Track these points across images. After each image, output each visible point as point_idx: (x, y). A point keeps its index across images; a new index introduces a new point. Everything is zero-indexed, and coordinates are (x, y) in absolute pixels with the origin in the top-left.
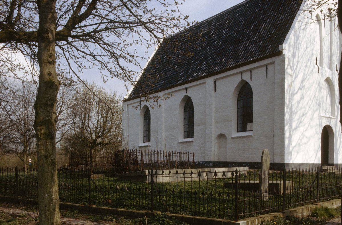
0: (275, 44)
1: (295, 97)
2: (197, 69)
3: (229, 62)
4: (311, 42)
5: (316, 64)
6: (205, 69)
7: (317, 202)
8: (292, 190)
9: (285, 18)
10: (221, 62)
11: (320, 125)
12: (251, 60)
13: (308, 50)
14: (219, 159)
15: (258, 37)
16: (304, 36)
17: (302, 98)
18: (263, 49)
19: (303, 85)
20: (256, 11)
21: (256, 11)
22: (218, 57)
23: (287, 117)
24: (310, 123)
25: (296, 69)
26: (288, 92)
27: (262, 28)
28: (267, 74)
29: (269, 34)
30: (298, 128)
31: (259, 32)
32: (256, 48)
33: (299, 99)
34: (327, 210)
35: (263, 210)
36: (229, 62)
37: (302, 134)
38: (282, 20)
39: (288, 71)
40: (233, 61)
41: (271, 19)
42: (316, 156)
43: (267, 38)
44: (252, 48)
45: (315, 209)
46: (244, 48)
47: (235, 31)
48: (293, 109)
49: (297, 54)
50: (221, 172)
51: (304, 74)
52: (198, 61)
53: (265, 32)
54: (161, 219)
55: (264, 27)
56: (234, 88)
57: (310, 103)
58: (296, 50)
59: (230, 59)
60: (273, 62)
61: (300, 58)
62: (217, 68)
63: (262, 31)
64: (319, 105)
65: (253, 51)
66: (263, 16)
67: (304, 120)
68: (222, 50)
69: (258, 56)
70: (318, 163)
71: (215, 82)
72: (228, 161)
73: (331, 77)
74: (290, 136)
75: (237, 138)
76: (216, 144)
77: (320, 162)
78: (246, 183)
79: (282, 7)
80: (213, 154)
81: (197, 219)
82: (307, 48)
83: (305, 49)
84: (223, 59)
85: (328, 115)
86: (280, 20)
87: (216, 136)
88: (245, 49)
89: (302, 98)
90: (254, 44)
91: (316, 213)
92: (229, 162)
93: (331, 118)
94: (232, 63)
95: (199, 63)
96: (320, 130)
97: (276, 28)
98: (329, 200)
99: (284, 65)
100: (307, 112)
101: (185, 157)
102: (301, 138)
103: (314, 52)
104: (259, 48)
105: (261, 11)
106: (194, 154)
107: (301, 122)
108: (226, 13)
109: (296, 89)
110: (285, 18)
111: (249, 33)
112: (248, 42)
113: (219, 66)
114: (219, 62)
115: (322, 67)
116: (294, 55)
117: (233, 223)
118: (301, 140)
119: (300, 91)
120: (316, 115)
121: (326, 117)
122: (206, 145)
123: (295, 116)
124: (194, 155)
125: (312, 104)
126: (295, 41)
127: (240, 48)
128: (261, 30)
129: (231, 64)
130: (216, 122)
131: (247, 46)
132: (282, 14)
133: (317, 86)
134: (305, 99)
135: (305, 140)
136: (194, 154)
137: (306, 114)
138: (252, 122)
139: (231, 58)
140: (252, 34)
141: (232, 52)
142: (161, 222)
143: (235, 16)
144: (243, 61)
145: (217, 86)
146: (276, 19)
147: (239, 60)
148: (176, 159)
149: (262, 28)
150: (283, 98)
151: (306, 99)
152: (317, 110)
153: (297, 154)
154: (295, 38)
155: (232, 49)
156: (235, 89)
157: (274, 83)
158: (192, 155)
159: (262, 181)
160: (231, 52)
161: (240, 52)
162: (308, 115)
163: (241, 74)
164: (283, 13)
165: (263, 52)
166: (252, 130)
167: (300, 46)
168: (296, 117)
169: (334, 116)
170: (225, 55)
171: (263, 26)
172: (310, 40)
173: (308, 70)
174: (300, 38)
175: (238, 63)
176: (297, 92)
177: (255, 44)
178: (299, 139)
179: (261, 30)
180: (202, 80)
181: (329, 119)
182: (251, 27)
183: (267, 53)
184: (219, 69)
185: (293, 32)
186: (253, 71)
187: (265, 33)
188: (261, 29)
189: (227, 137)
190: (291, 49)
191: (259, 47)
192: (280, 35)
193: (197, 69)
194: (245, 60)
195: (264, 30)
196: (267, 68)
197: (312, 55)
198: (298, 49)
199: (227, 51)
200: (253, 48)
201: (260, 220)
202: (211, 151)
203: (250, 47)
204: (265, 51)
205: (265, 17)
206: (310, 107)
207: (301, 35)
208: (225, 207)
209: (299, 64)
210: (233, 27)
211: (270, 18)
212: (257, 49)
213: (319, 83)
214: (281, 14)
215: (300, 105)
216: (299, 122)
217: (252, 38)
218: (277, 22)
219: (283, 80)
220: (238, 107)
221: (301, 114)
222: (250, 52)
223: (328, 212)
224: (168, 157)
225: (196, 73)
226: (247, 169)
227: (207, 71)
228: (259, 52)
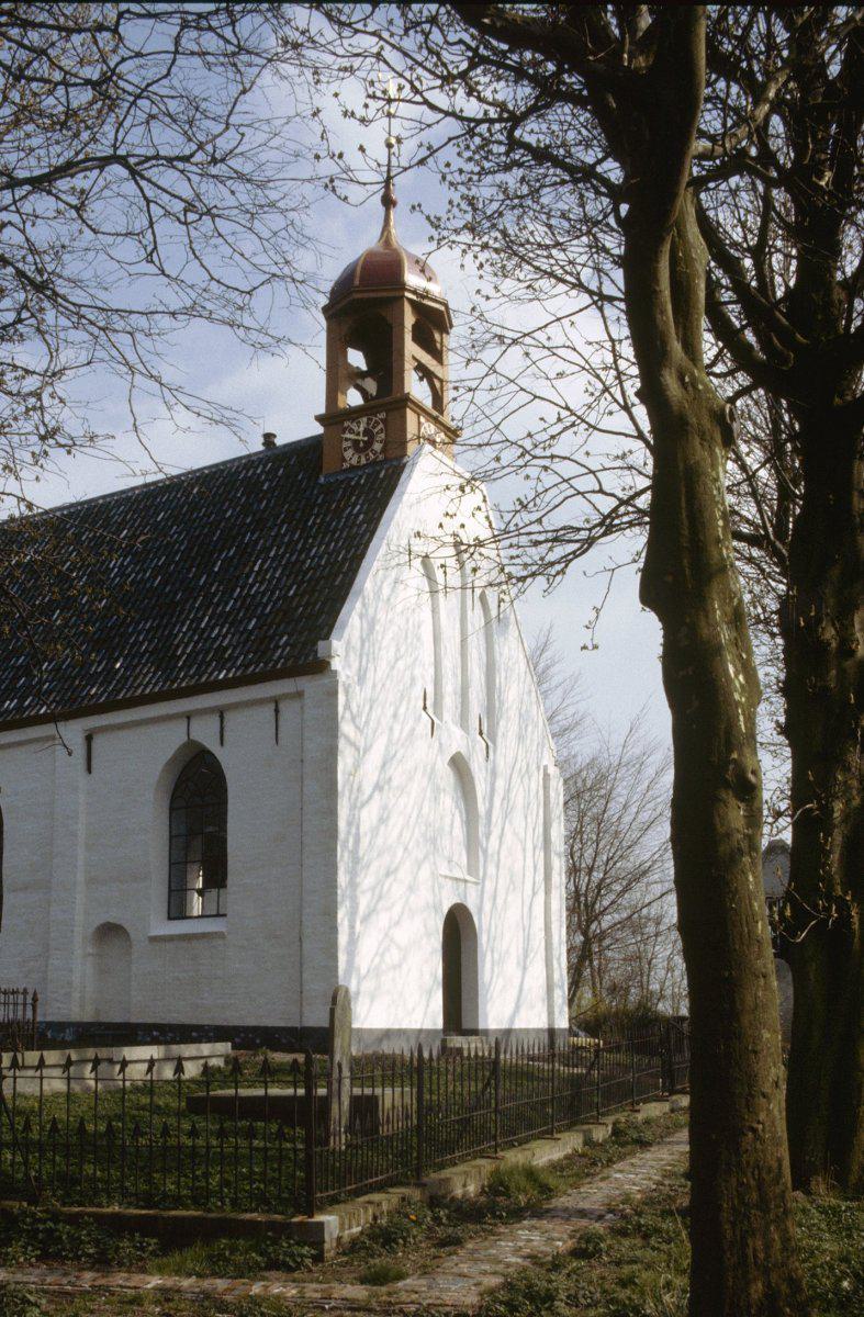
0: (301, 633)
1: (364, 814)
2: (18, 686)
3: (139, 674)
4: (409, 641)
5: (425, 708)
6: (49, 692)
7: (496, 1152)
8: (400, 1124)
9: (330, 554)
10: (110, 671)
11: (436, 908)
12: (221, 676)
13: (401, 664)
14: (97, 1011)
15: (239, 603)
16: (390, 621)
17: (383, 820)
18: (261, 643)
19: (387, 777)
20: (229, 514)
21: (229, 514)
22: (98, 652)
23: (342, 878)
24: (407, 901)
25: (367, 723)
26: (347, 793)
27: (253, 576)
28: (277, 729)
29: (278, 599)
30: (374, 917)
31: (242, 588)
32: (237, 637)
33: (375, 821)
34: (530, 1174)
35: (371, 1181)
36: (139, 674)
37: (386, 935)
38: (321, 558)
39: (346, 728)
40: (155, 673)
41: (282, 550)
42: (428, 1005)
43: (274, 610)
44: (223, 636)
45: (496, 1172)
46: (194, 634)
47: (157, 570)
48: (361, 853)
49: (370, 674)
50: (144, 1061)
51: (390, 740)
52: (18, 659)
53: (263, 588)
54: (41, 1227)
55: (258, 573)
56: (160, 768)
57: (406, 835)
58: (368, 661)
59: (145, 665)
60: (298, 692)
61: (378, 689)
62: (94, 689)
63: (252, 586)
64: (433, 841)
65: (226, 649)
66: (252, 534)
67: (389, 890)
68: (111, 628)
69: (247, 667)
70: (428, 1025)
71: (89, 739)
72: (134, 1020)
73: (464, 751)
74: (353, 941)
75: (171, 938)
76: (90, 958)
77: (440, 1024)
78: (242, 1099)
79: (317, 516)
80: (76, 995)
81: (176, 1217)
82: (397, 660)
83: (393, 661)
84: (117, 661)
85: (459, 875)
86: (313, 559)
87: (91, 930)
88: (196, 638)
89: (383, 820)
90: (227, 625)
91: (502, 1184)
92: (138, 1026)
93: (466, 881)
94: (149, 680)
95: (21, 665)
96: (437, 925)
97: (302, 582)
98: (516, 1144)
99: (335, 706)
100: (400, 863)
101: (20, 1008)
102: (381, 951)
103: (417, 672)
104: (247, 640)
105: (246, 516)
106: (35, 994)
107: (380, 897)
108: (119, 503)
109: (367, 790)
110: (330, 554)
111: (209, 584)
112: (204, 615)
113: (101, 685)
114: (103, 669)
115: (494, 743)
116: (361, 679)
117: (301, 1223)
118: (383, 955)
119: (377, 795)
120: (425, 873)
121: (451, 878)
122: (51, 961)
123: (365, 877)
124: (35, 999)
125: (413, 840)
126: (364, 636)
127: (179, 631)
128: (251, 581)
129: (148, 683)
130: (91, 881)
131: (203, 626)
132: (319, 539)
133: (426, 780)
134: (391, 822)
135: (394, 956)
136: (35, 994)
137: (396, 869)
138: (225, 886)
139: (147, 662)
140: (217, 590)
141: (150, 642)
142: (40, 1236)
143: (152, 517)
144: (192, 677)
145: (94, 755)
146: (300, 553)
147: (179, 673)
148: (20, 1013)
149: (253, 576)
150: (332, 813)
151: (396, 822)
152: (426, 857)
153: (372, 1002)
154: (365, 625)
155: (148, 631)
156: (163, 771)
157: (302, 761)
158: (29, 1000)
159: (335, 1086)
160: (144, 640)
161: (178, 646)
162: (401, 874)
163: (186, 720)
164: (323, 538)
165: (264, 653)
166: (225, 915)
167: (380, 649)
168: (367, 881)
169: (477, 876)
170: (124, 648)
171: (256, 568)
172: (406, 633)
173: (402, 729)
174: (377, 628)
175: (173, 682)
176: (370, 797)
177: (231, 624)
178: (376, 954)
179: (251, 581)
180: (36, 728)
181: (462, 885)
182: (214, 565)
183: (277, 662)
184: (102, 695)
185: (358, 605)
186: (227, 716)
187: (264, 594)
188: (248, 577)
189: (132, 936)
190: (353, 657)
191: (245, 635)
192: (318, 607)
193: (18, 686)
194: (201, 677)
195: (261, 583)
196: (277, 711)
197: (413, 679)
198: (374, 658)
199: (131, 635)
200: (225, 637)
201: (370, 1211)
202: (70, 983)
203: (216, 631)
204: (269, 653)
205: (259, 538)
206: (406, 849)
207: (381, 616)
208: (245, 1178)
209: (375, 707)
210: (149, 554)
211: (279, 548)
212: (238, 643)
213: (433, 769)
214: (315, 538)
215: (380, 841)
216: (376, 897)
217: (218, 605)
218: (304, 562)
219: (332, 753)
220: (170, 832)
221: (382, 872)
222: (217, 650)
223: (535, 1181)
224: (29, 1008)
225: (12, 701)
226: (224, 1048)
227: (58, 699)
228: (248, 652)
